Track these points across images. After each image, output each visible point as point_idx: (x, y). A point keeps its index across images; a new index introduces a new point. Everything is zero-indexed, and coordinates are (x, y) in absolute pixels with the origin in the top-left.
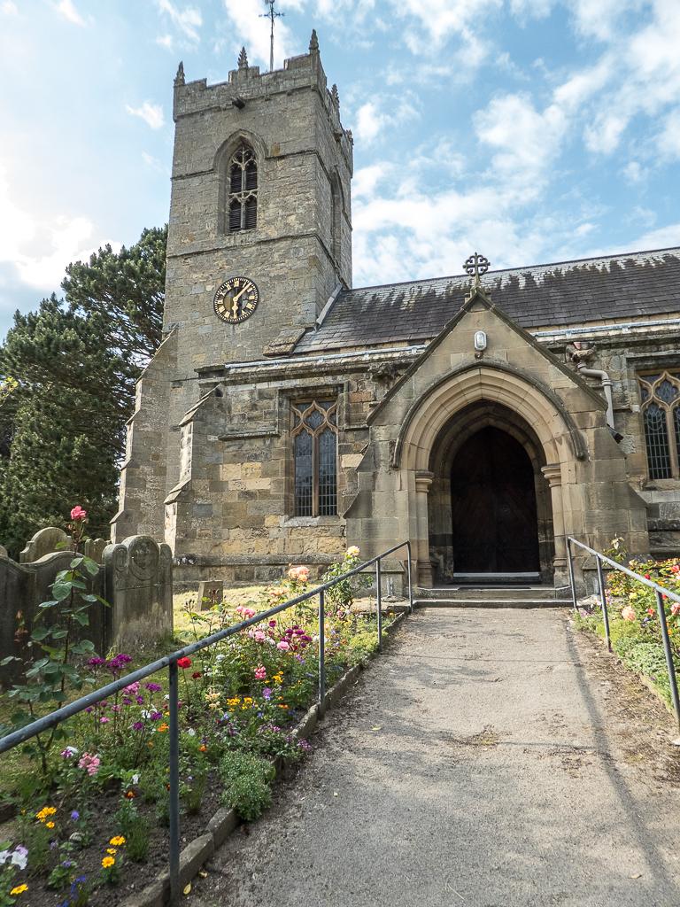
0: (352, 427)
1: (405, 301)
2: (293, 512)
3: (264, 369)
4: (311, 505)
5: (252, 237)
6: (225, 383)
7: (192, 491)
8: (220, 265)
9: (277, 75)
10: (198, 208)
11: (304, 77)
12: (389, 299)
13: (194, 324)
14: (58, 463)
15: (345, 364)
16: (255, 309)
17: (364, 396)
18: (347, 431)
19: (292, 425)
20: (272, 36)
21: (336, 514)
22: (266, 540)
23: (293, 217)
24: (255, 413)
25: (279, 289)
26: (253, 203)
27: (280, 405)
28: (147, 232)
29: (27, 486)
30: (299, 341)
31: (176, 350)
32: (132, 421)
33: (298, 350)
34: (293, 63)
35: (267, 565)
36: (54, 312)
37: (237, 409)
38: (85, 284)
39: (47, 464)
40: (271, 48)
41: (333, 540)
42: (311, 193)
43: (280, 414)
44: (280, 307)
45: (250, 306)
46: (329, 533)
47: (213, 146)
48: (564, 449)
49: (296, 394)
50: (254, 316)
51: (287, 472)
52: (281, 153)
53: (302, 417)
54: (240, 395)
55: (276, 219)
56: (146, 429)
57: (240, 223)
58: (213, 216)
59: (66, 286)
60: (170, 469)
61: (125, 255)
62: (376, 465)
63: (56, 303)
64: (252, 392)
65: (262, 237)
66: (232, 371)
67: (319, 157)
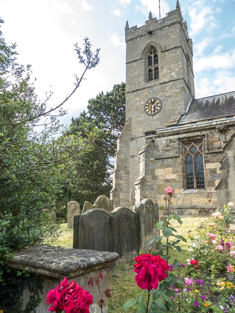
0: (210, 152)
1: (221, 102)
2: (186, 187)
3: (171, 130)
4: (194, 184)
5: (157, 82)
6: (156, 137)
8: (146, 94)
9: (164, 19)
10: (136, 73)
11: (175, 18)
12: (214, 101)
13: (137, 117)
14: (89, 171)
15: (205, 126)
16: (161, 109)
18: (208, 154)
19: (184, 152)
20: (159, 7)
21: (204, 188)
22: (175, 198)
23: (173, 73)
24: (168, 148)
25: (170, 101)
26: (157, 69)
27: (179, 144)
28: (115, 86)
29: (78, 179)
30: (179, 120)
31: (131, 127)
32: (116, 154)
33: (180, 123)
34: (170, 14)
35: (177, 209)
36: (85, 117)
37: (161, 147)
38: (95, 106)
39: (85, 171)
40: (161, 12)
41: (204, 199)
42: (180, 63)
43: (179, 148)
44: (170, 108)
45: (158, 108)
46: (202, 196)
47: (141, 50)
49: (185, 140)
50: (160, 112)
51: (183, 171)
52: (167, 49)
53: (188, 149)
54: (162, 142)
55: (167, 74)
56: (122, 157)
57: (152, 77)
58: (142, 76)
59: (89, 107)
61: (108, 95)
62: (228, 167)
63: (85, 114)
64: (166, 140)
65: (162, 82)
66: (158, 132)
67: (182, 48)
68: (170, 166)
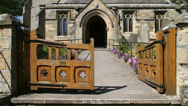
17: (73, 13)
18: (70, 20)
24: (51, 15)
33: (59, 3)
48: (110, 25)
54: (48, 12)
62: (76, 26)
68: (51, 23)
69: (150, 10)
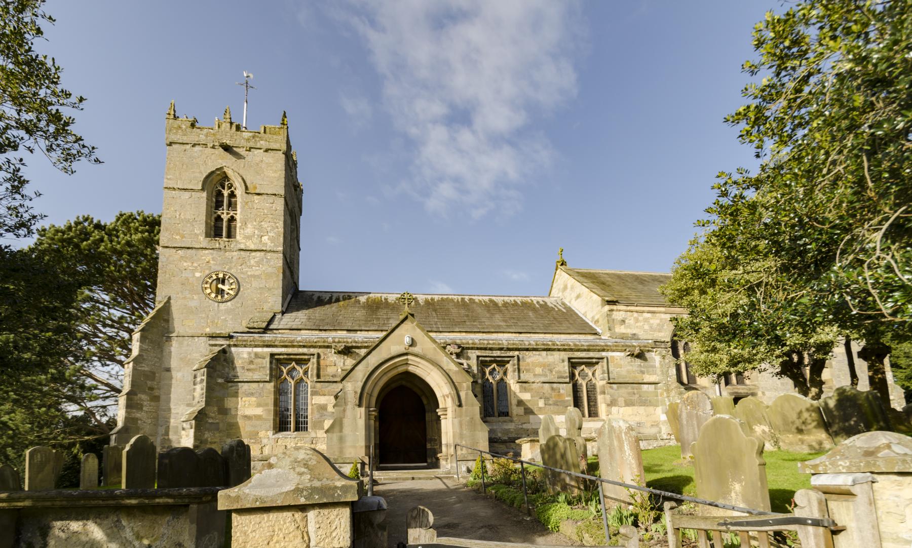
7: (206, 414)
13: (185, 298)
24: (252, 367)
47: (201, 172)
60: (163, 397)
62: (346, 404)
64: (249, 353)
68: (252, 394)
69: (557, 355)
